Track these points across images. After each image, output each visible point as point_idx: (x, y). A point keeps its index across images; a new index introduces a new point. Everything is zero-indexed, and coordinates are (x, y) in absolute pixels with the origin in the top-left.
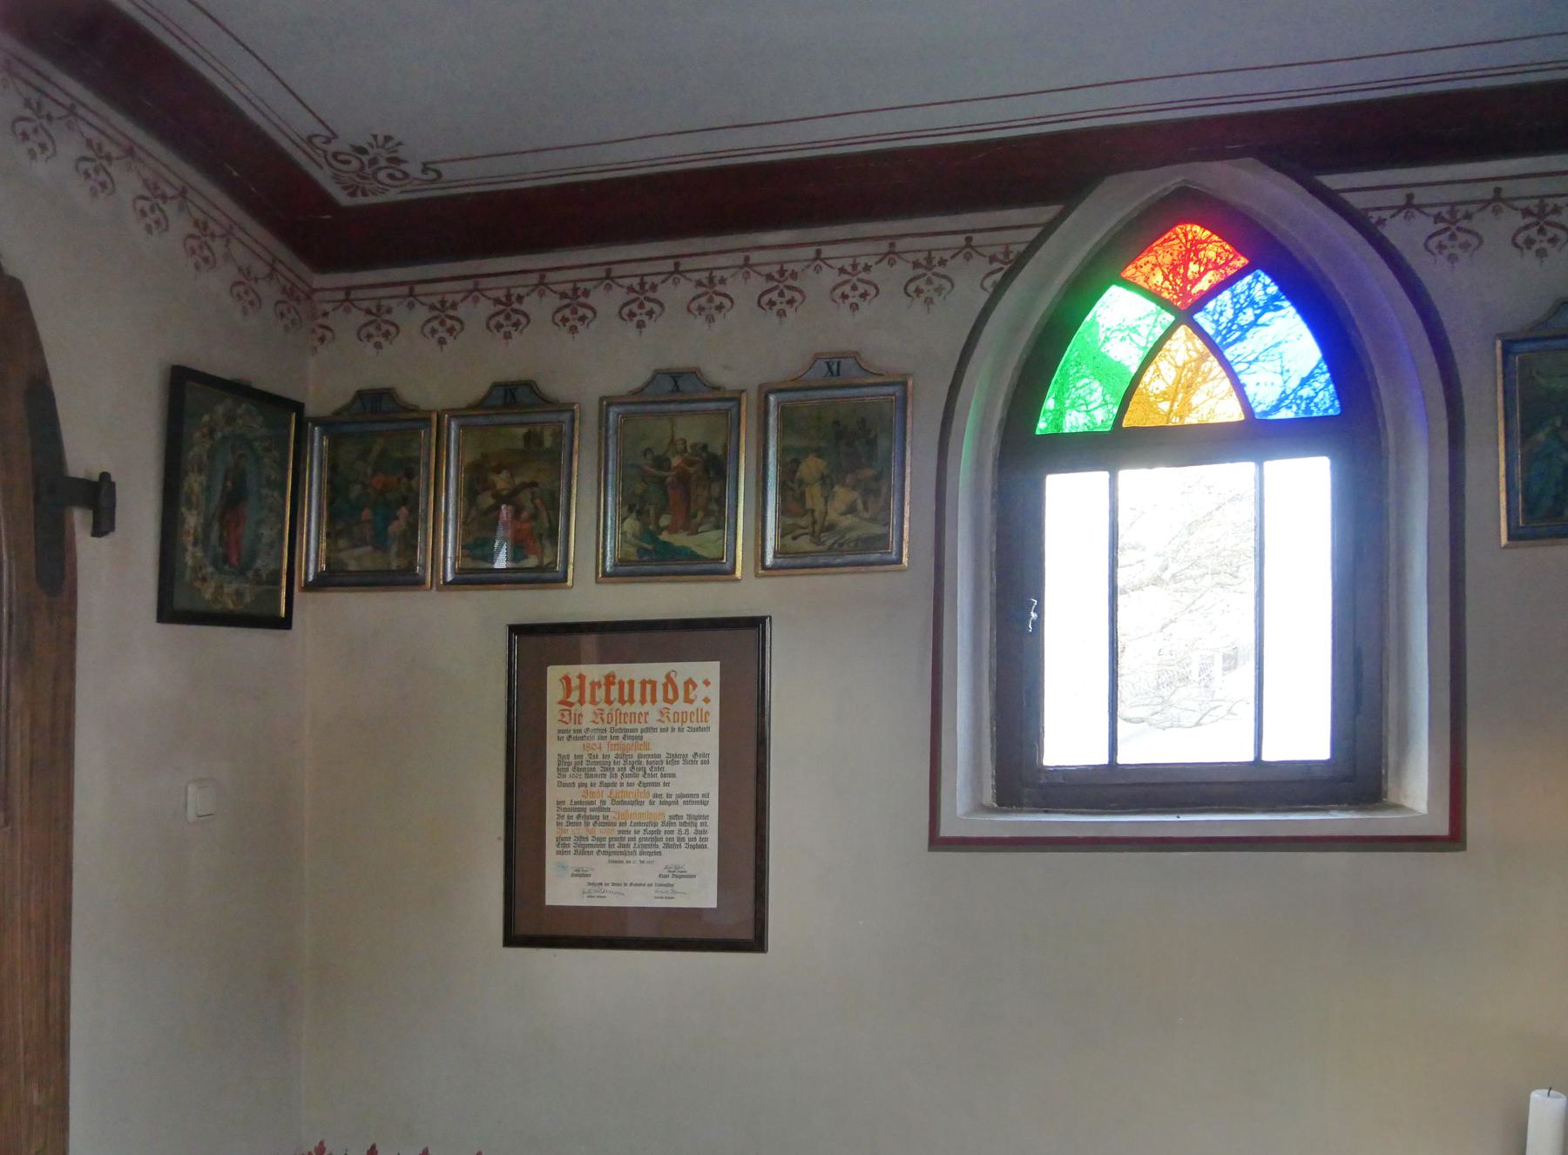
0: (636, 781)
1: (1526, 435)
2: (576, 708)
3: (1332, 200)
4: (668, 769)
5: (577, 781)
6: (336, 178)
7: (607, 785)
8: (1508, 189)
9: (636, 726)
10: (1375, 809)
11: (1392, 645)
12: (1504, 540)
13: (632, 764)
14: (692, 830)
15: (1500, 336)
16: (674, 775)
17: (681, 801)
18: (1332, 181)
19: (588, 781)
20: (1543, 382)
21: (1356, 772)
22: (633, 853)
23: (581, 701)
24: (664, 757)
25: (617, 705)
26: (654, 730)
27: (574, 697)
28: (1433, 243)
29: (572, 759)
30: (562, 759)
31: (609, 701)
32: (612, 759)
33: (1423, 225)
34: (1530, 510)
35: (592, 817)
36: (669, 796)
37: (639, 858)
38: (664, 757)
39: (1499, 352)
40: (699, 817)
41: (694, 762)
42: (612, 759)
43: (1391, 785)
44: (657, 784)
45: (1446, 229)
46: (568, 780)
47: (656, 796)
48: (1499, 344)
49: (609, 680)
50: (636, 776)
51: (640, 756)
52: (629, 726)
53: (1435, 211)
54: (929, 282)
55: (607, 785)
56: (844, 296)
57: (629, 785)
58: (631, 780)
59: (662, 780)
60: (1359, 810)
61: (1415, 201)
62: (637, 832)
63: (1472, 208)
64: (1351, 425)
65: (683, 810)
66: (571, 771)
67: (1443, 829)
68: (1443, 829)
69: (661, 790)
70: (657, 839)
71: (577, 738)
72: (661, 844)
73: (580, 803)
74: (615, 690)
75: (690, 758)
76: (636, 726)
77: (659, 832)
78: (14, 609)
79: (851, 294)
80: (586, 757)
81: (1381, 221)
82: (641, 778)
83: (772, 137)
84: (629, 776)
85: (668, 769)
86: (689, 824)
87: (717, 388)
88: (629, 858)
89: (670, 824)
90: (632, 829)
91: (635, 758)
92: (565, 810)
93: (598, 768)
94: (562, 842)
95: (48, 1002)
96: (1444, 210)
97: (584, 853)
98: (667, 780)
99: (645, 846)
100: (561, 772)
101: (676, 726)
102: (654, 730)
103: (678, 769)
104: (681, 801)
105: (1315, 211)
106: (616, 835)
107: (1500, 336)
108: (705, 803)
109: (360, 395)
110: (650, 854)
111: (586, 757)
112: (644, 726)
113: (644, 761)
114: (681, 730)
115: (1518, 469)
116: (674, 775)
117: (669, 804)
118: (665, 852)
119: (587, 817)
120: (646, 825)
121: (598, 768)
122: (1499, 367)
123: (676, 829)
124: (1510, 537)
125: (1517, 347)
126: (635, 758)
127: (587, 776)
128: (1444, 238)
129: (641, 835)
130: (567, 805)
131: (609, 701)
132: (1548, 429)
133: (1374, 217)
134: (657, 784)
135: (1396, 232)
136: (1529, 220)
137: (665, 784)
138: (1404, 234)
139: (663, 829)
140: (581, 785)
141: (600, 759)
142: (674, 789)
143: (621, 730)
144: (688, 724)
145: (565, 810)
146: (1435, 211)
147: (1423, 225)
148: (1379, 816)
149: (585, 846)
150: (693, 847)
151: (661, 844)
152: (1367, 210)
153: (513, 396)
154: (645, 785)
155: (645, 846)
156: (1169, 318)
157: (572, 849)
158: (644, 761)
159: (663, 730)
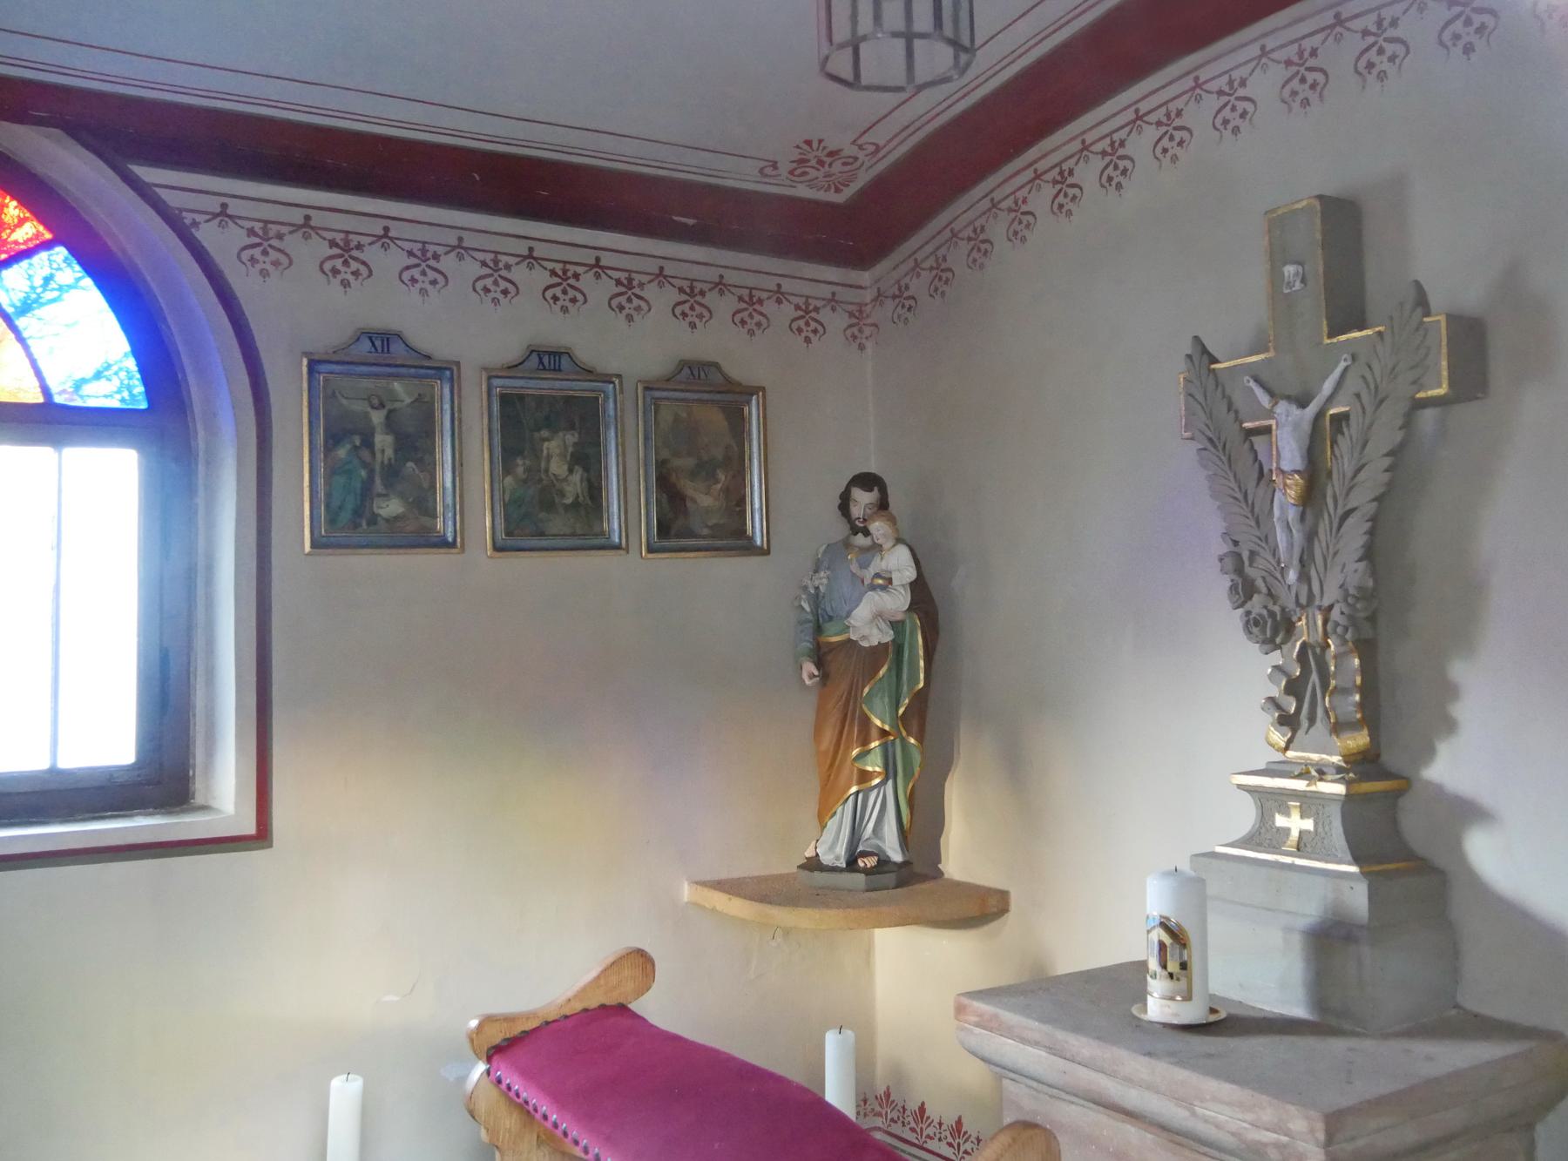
1: (328, 450)
3: (144, 191)
6: (811, 184)
8: (318, 219)
10: (184, 811)
11: (199, 644)
12: (307, 548)
15: (305, 354)
18: (148, 174)
20: (344, 402)
21: (164, 778)
28: (246, 255)
33: (236, 236)
34: (332, 521)
39: (305, 369)
43: (198, 785)
45: (417, 265)
48: (305, 362)
53: (248, 224)
54: (265, 253)
56: (555, 299)
60: (170, 813)
61: (465, 244)
63: (284, 230)
64: (163, 415)
67: (250, 829)
68: (250, 829)
79: (492, 288)
81: (195, 224)
83: (81, 60)
87: (428, 357)
96: (258, 226)
105: (127, 195)
107: (305, 354)
109: (684, 364)
115: (321, 481)
122: (305, 385)
124: (313, 545)
125: (323, 368)
128: (257, 252)
132: (348, 446)
133: (188, 218)
135: (207, 234)
136: (336, 251)
138: (221, 242)
146: (248, 224)
147: (236, 236)
148: (187, 819)
152: (181, 210)
153: (697, 376)
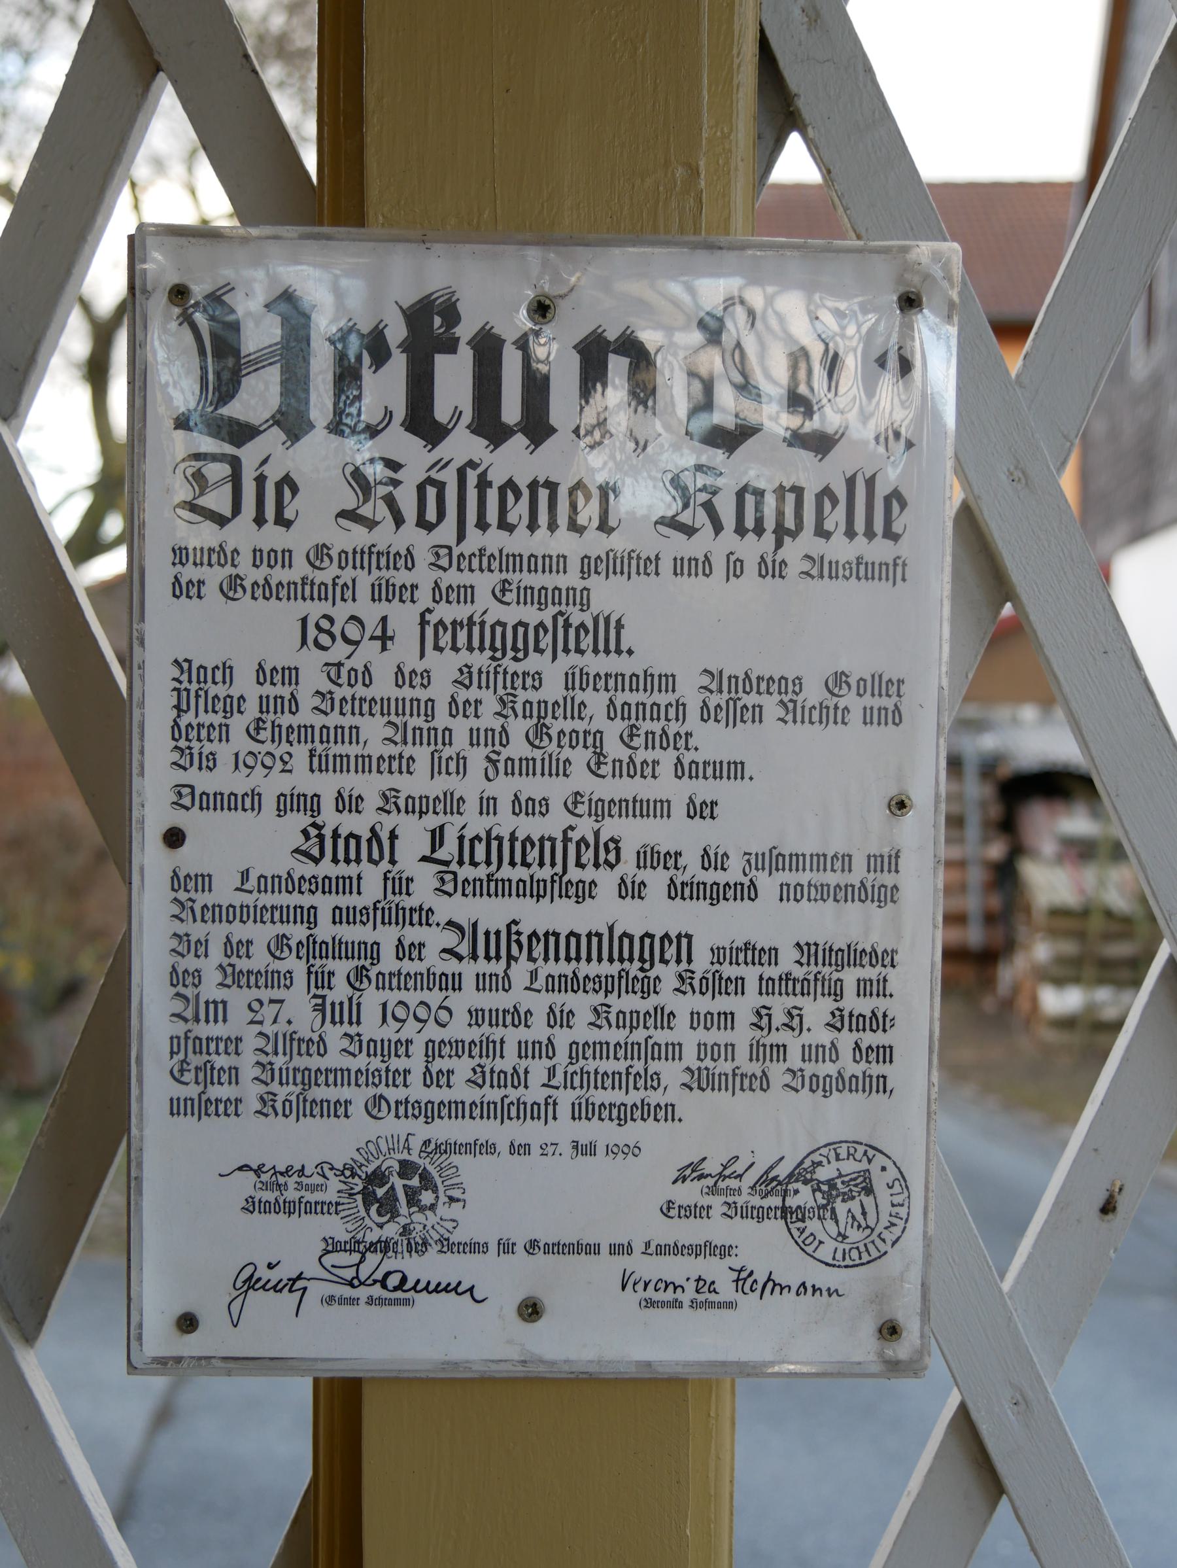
0: (556, 790)
2: (268, 452)
4: (713, 741)
5: (273, 785)
7: (418, 807)
9: (563, 542)
13: (540, 714)
14: (817, 1010)
16: (736, 770)
17: (768, 884)
19: (327, 785)
22: (544, 1111)
23: (292, 423)
24: (689, 691)
25: (463, 445)
26: (648, 565)
27: (259, 397)
29: (245, 684)
30: (195, 682)
31: (423, 423)
32: (441, 690)
35: (339, 949)
36: (711, 859)
37: (564, 1129)
38: (689, 691)
40: (853, 956)
41: (832, 715)
42: (441, 690)
44: (660, 808)
46: (224, 779)
47: (649, 857)
49: (430, 327)
50: (562, 769)
51: (575, 680)
52: (521, 542)
55: (418, 807)
57: (523, 806)
58: (533, 787)
59: (677, 791)
62: (560, 1018)
65: (774, 922)
66: (240, 742)
69: (682, 836)
70: (655, 1051)
71: (268, 591)
72: (671, 1073)
73: (291, 884)
74: (453, 381)
75: (813, 694)
76: (563, 542)
77: (664, 1017)
78: (931, 1230)
80: (313, 678)
82: (580, 780)
84: (526, 767)
85: (713, 741)
86: (803, 987)
88: (531, 1132)
89: (716, 984)
90: (539, 1004)
91: (553, 690)
92: (215, 913)
93: (374, 729)
94: (197, 1059)
95: (268, 238)
97: (307, 1108)
98: (705, 790)
99: (601, 1080)
100: (189, 747)
101: (752, 549)
102: (648, 565)
103: (769, 743)
104: (768, 884)
106: (460, 1029)
108: (888, 896)
110: (622, 1115)
111: (313, 678)
112: (596, 543)
113: (596, 702)
114: (771, 569)
116: (736, 770)
117: (716, 894)
118: (690, 1104)
119: (312, 948)
120: (605, 985)
121: (374, 729)
123: (743, 1006)
126: (553, 690)
127: (319, 764)
129: (582, 1032)
130: (224, 893)
131: (423, 423)
134: (660, 808)
137: (702, 810)
139: (683, 1005)
140: (288, 803)
141: (383, 687)
142: (741, 828)
143: (484, 560)
144: (807, 542)
145: (215, 913)
149: (309, 1078)
150: (818, 1085)
151: (671, 1073)
154: (601, 809)
155: (601, 1080)
156: (224, 298)
157: (251, 1092)
158: (596, 702)
159: (682, 566)
